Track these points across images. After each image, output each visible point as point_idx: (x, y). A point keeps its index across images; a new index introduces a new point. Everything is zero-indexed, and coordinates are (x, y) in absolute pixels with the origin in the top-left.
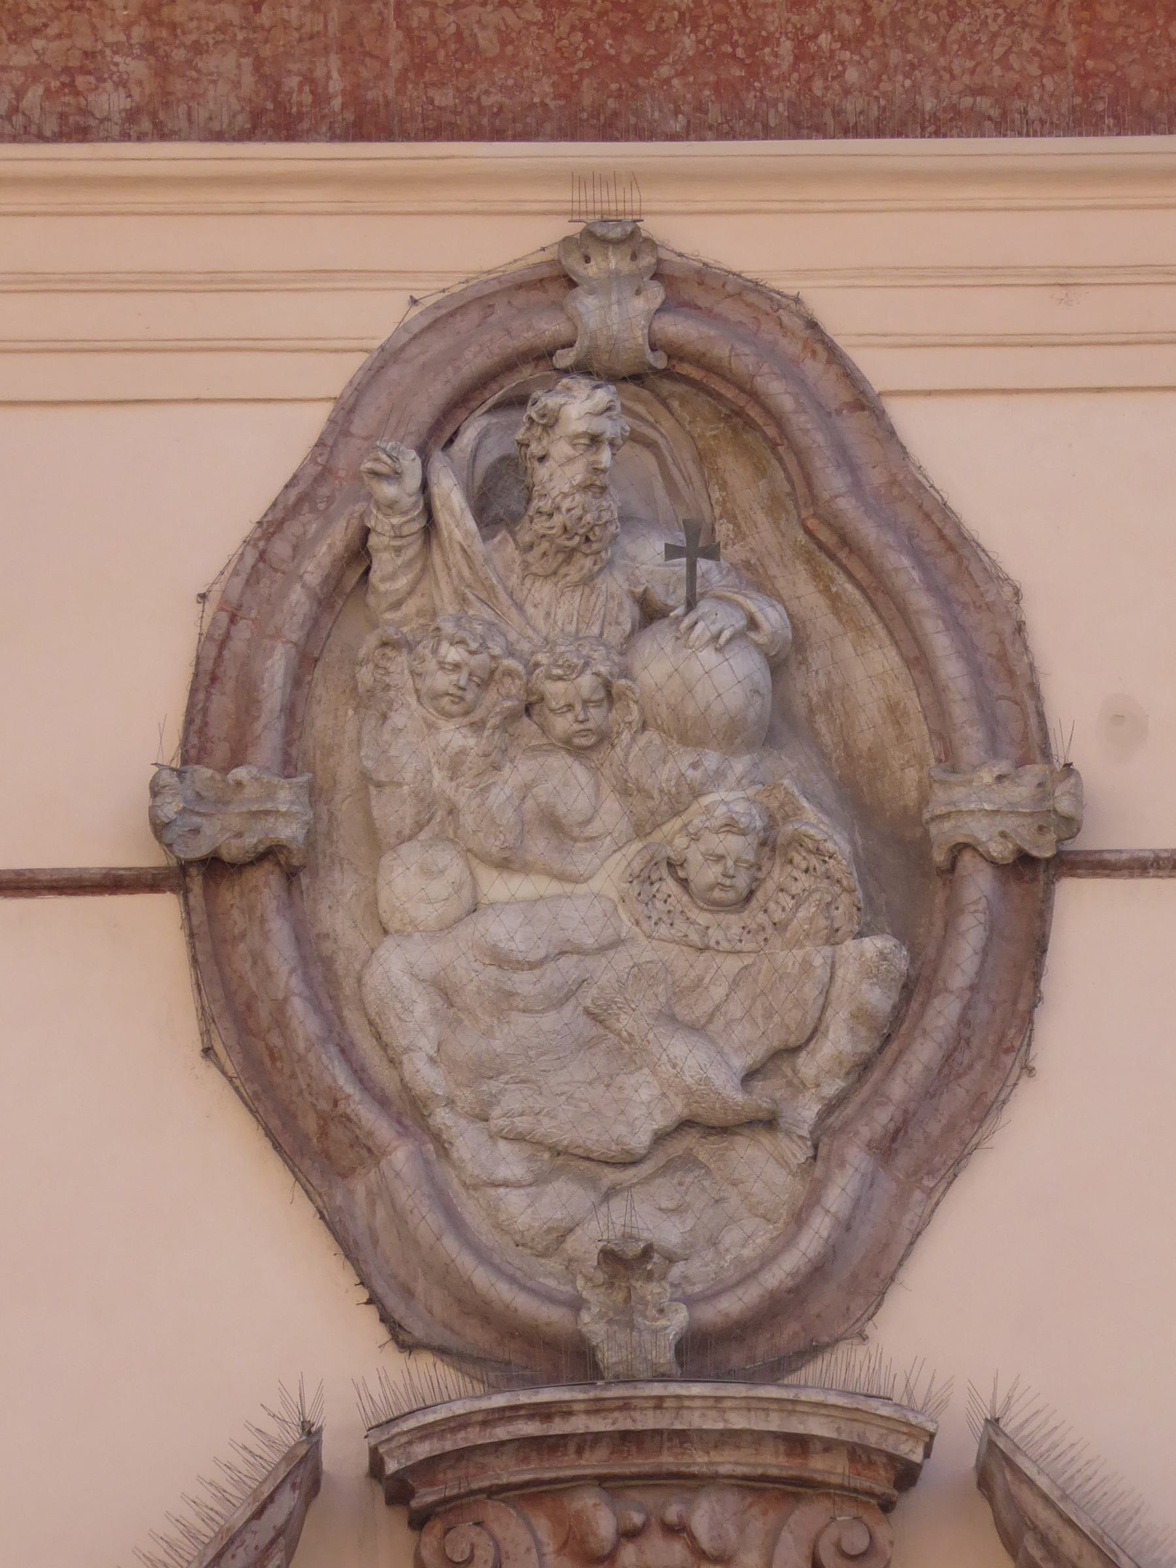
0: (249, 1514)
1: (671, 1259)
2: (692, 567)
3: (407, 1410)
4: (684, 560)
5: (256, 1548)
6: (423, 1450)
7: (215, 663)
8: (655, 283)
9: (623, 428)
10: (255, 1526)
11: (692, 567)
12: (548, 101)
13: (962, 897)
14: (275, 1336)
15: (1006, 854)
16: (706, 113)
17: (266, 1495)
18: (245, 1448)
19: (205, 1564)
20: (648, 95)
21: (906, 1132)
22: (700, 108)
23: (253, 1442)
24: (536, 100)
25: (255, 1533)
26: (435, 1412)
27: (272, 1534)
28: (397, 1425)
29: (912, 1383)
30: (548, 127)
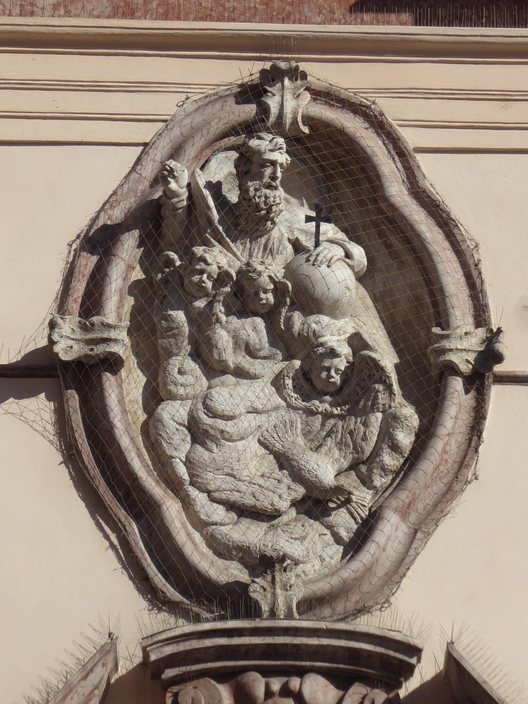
0: (80, 677)
1: (297, 563)
2: (318, 227)
3: (161, 630)
4: (315, 223)
5: (83, 695)
6: (169, 650)
7: (203, 492)
8: (306, 92)
9: (287, 159)
10: (83, 683)
11: (318, 227)
12: (257, 6)
13: (431, 368)
14: (107, 610)
15: (468, 371)
16: (334, 13)
17: (89, 668)
18: (80, 646)
19: (57, 701)
20: (306, 5)
21: (414, 505)
22: (332, 11)
23: (86, 644)
24: (252, 5)
25: (83, 687)
26: (175, 631)
27: (91, 688)
28: (156, 637)
29: (412, 624)
30: (257, 18)
